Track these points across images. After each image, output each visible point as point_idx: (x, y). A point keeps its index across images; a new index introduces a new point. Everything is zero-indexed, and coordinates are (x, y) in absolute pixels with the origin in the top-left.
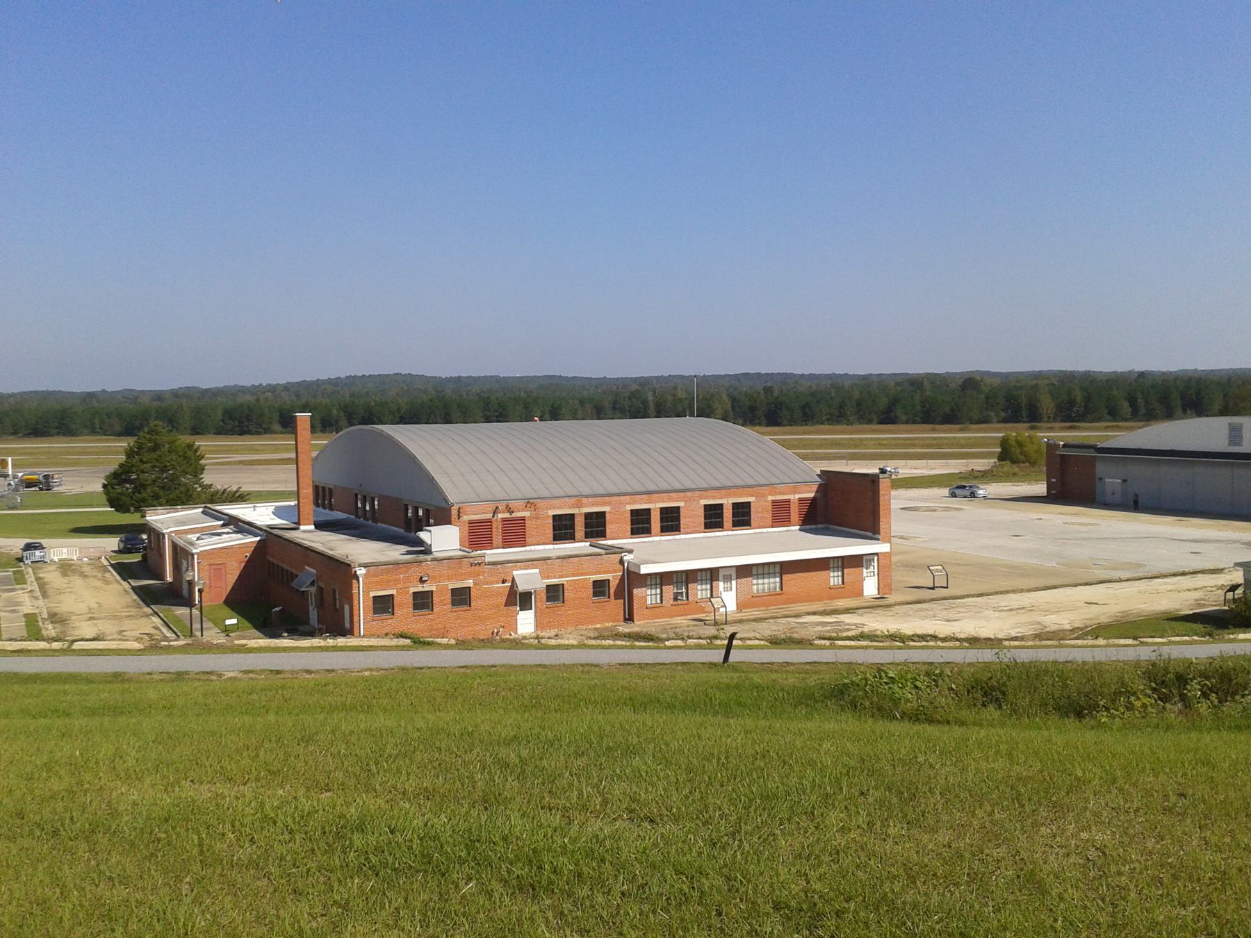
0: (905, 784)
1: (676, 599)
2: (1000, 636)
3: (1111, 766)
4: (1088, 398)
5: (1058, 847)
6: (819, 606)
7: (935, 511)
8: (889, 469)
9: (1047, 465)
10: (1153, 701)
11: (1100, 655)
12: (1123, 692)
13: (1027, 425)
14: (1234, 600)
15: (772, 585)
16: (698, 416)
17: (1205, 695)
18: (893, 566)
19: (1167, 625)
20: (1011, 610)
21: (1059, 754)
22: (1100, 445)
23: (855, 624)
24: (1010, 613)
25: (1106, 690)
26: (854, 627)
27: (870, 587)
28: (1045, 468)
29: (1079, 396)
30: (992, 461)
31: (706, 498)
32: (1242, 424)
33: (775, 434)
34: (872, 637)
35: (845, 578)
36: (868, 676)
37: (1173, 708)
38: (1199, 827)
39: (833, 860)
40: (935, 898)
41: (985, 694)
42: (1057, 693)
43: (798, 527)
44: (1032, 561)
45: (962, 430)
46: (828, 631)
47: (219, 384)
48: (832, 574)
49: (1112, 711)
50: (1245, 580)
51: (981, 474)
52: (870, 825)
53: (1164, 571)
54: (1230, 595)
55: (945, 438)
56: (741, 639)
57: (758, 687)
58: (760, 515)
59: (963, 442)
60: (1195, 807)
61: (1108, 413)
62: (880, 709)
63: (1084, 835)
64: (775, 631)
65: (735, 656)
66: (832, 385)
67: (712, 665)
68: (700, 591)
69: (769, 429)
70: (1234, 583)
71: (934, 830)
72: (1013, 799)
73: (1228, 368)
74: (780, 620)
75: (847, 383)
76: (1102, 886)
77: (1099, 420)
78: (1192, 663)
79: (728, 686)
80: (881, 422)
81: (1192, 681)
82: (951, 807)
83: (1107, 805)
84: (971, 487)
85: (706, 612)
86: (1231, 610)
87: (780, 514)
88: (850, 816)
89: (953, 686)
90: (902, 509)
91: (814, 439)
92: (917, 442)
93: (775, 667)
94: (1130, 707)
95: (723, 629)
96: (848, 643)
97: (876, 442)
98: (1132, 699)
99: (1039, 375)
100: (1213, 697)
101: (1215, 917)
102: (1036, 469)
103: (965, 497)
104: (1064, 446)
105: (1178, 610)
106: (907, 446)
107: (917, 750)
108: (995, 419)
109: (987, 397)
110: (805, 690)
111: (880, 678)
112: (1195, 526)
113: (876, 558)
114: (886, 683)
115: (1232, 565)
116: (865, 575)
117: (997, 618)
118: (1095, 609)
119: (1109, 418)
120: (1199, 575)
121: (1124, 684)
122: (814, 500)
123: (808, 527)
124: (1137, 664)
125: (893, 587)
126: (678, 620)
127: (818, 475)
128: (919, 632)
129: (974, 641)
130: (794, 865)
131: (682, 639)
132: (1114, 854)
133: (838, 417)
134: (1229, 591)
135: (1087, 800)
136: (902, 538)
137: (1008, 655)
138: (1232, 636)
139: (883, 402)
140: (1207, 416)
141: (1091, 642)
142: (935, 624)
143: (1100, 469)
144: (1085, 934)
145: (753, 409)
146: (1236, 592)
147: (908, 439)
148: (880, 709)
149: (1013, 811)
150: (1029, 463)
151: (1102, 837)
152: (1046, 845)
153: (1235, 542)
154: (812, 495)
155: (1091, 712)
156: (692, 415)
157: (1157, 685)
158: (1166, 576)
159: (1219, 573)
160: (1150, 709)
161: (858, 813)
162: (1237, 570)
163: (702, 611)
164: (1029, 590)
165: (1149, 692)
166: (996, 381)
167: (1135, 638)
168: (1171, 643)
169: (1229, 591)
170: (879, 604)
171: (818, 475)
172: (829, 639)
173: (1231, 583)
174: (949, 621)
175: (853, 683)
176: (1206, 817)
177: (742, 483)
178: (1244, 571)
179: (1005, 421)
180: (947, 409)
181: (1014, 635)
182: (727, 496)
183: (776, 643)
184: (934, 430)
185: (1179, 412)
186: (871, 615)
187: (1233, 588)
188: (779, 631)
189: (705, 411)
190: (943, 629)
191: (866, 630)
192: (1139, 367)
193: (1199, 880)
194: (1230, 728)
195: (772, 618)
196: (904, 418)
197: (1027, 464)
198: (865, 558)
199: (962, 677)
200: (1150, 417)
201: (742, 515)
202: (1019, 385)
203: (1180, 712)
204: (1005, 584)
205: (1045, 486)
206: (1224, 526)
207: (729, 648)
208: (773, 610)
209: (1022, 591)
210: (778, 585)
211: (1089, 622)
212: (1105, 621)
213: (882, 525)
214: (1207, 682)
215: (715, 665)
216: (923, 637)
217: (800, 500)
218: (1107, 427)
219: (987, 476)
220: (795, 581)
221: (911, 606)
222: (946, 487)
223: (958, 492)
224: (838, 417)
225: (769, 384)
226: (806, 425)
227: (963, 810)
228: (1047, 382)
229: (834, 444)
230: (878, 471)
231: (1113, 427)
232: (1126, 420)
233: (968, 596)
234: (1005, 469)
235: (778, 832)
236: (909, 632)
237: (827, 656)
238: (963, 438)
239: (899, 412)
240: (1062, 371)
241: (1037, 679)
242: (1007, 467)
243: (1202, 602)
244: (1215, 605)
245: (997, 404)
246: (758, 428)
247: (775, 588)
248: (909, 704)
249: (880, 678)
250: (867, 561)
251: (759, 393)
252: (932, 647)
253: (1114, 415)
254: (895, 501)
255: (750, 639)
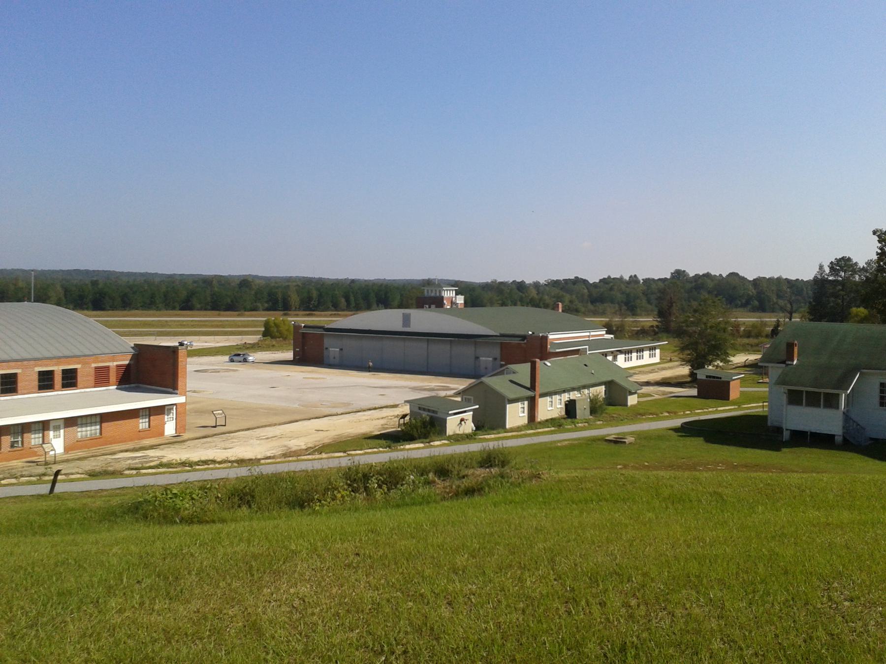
0: (171, 571)
1: (12, 446)
2: (259, 457)
3: (314, 540)
4: (320, 296)
5: (274, 601)
6: (130, 445)
7: (219, 372)
8: (185, 343)
9: (294, 340)
10: (348, 493)
11: (317, 465)
12: (330, 488)
13: (282, 313)
14: (404, 424)
15: (93, 432)
16: (35, 301)
17: (380, 487)
18: (188, 413)
19: (364, 442)
20: (267, 438)
21: (282, 535)
22: (327, 326)
23: (158, 457)
24: (268, 440)
25: (319, 488)
26: (156, 459)
27: (170, 428)
28: (292, 341)
29: (315, 294)
30: (259, 337)
31: (41, 366)
32: (410, 314)
33: (99, 317)
34: (169, 465)
35: (151, 423)
36: (157, 494)
37: (361, 496)
38: (366, 575)
39: (109, 635)
40: (184, 650)
41: (241, 499)
42: (288, 493)
43: (116, 387)
44: (284, 404)
45: (239, 315)
46: (136, 463)
47: (126, 270)
48: (141, 421)
49: (322, 502)
50: (411, 411)
51: (251, 346)
52: (142, 604)
53: (364, 407)
54: (402, 421)
55: (227, 321)
56: (65, 474)
57: (73, 511)
58: (84, 379)
59: (240, 323)
60: (364, 561)
61: (332, 306)
62: (165, 517)
63: (292, 591)
64: (95, 466)
65: (59, 488)
66: (145, 281)
67: (40, 497)
68: (34, 439)
69: (95, 313)
70: (404, 413)
71: (188, 602)
72: (246, 571)
73: (403, 278)
74: (98, 458)
75: (157, 280)
76: (301, 624)
77: (327, 309)
78: (372, 466)
79: (46, 512)
80: (182, 309)
81: (372, 477)
82: (202, 583)
83: (309, 567)
84: (244, 355)
85: (39, 455)
86: (402, 430)
87: (101, 377)
88: (126, 600)
89: (219, 495)
90: (195, 371)
91: (131, 321)
92: (207, 323)
93: (92, 494)
94: (334, 498)
95: (50, 468)
96: (150, 471)
97: (178, 323)
98: (336, 492)
99: (289, 279)
100: (385, 487)
101: (370, 634)
102: (287, 342)
103: (240, 362)
104: (304, 327)
105: (371, 432)
106: (201, 326)
107: (183, 545)
108: (261, 308)
109: (256, 294)
110: (108, 509)
111: (167, 494)
112: (383, 378)
113: (175, 407)
114: (171, 498)
115: (403, 402)
116: (166, 420)
117: (258, 444)
118: (322, 434)
119: (333, 308)
120: (384, 409)
121: (331, 483)
122: (128, 366)
123: (123, 386)
124: (339, 469)
125: (187, 427)
126: (14, 463)
127: (132, 348)
128: (203, 458)
129: (241, 462)
130: (79, 643)
131: (16, 478)
132: (311, 601)
133: (149, 304)
134: (401, 418)
135: (296, 565)
136: (194, 392)
137: (257, 470)
138: (402, 447)
139: (184, 294)
140: (391, 308)
141: (317, 456)
142: (216, 452)
143: (327, 342)
144: (286, 661)
145: (82, 297)
146: (406, 419)
147: (201, 321)
148: (165, 517)
149: (246, 580)
150: (283, 338)
151: (304, 590)
152: (267, 601)
153: (405, 387)
154: (127, 362)
155: (309, 504)
156: (29, 300)
157: (351, 482)
158: (364, 411)
159: (396, 407)
160: (346, 498)
161: (133, 597)
162: (406, 405)
163: (35, 454)
164: (280, 424)
165: (346, 487)
166: (263, 282)
167: (345, 452)
168: (366, 453)
169: (401, 418)
170: (176, 441)
171: (132, 348)
172: (136, 469)
173: (403, 413)
174: (225, 449)
175: (146, 501)
176: (371, 567)
177: (70, 354)
178: (410, 405)
179: (268, 309)
180: (229, 300)
181: (269, 455)
182: (56, 365)
183: (93, 476)
184: (219, 315)
185: (375, 306)
186: (170, 449)
187: (404, 416)
188: (97, 466)
189: (42, 297)
190: (218, 454)
191: (165, 460)
192: (352, 277)
193: (362, 611)
194: (393, 506)
195: (93, 456)
196: (199, 306)
197: (281, 339)
198: (166, 408)
199: (226, 488)
200: (358, 308)
201: (70, 379)
202: (277, 285)
203: (365, 499)
204: (264, 421)
205: (292, 353)
206: (400, 377)
207: (54, 482)
208: (93, 451)
209: (275, 425)
210: (98, 431)
211: (317, 443)
212: (329, 441)
213: (180, 383)
214: (381, 478)
215: (42, 496)
216: (205, 462)
217: (117, 366)
218: (331, 315)
219: (255, 347)
220: (111, 427)
221: (199, 440)
222: (227, 355)
223: (235, 358)
224: (149, 304)
225: (95, 279)
226: (125, 310)
227: (211, 584)
228: (294, 284)
229: (181, 324)
230: (177, 344)
231: (335, 314)
232: (343, 310)
233: (239, 431)
234: (267, 342)
235: (69, 619)
236: (196, 459)
237: (140, 481)
238: (239, 321)
239: (195, 301)
240: (304, 277)
241: (275, 485)
242: (269, 341)
243: (386, 426)
244: (392, 428)
245: (263, 298)
246: (86, 312)
247: (96, 434)
248: (187, 512)
249: (167, 494)
250: (168, 409)
251: (87, 285)
252: (212, 469)
253: (336, 307)
254: (190, 366)
255: (72, 474)
